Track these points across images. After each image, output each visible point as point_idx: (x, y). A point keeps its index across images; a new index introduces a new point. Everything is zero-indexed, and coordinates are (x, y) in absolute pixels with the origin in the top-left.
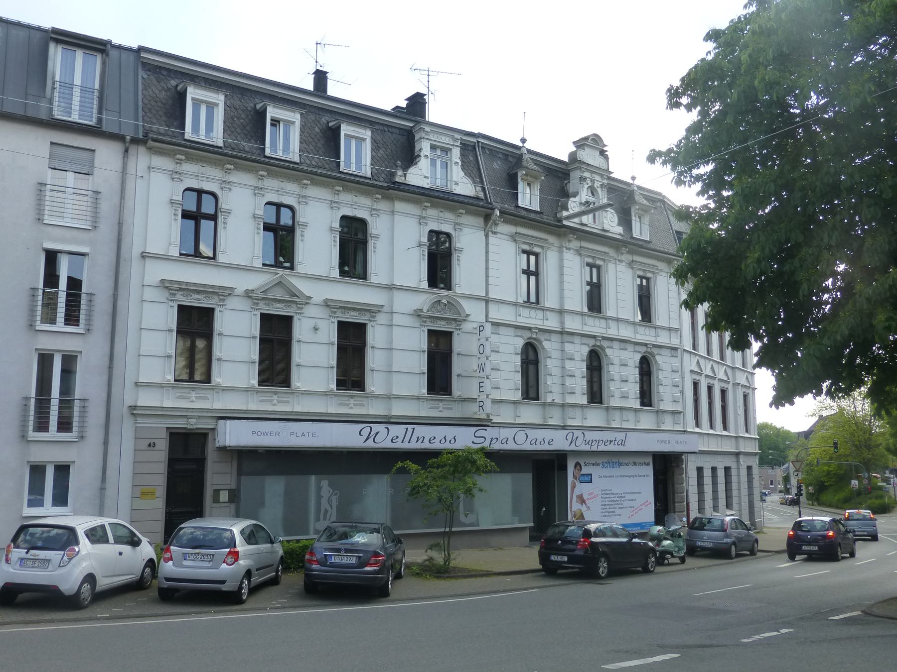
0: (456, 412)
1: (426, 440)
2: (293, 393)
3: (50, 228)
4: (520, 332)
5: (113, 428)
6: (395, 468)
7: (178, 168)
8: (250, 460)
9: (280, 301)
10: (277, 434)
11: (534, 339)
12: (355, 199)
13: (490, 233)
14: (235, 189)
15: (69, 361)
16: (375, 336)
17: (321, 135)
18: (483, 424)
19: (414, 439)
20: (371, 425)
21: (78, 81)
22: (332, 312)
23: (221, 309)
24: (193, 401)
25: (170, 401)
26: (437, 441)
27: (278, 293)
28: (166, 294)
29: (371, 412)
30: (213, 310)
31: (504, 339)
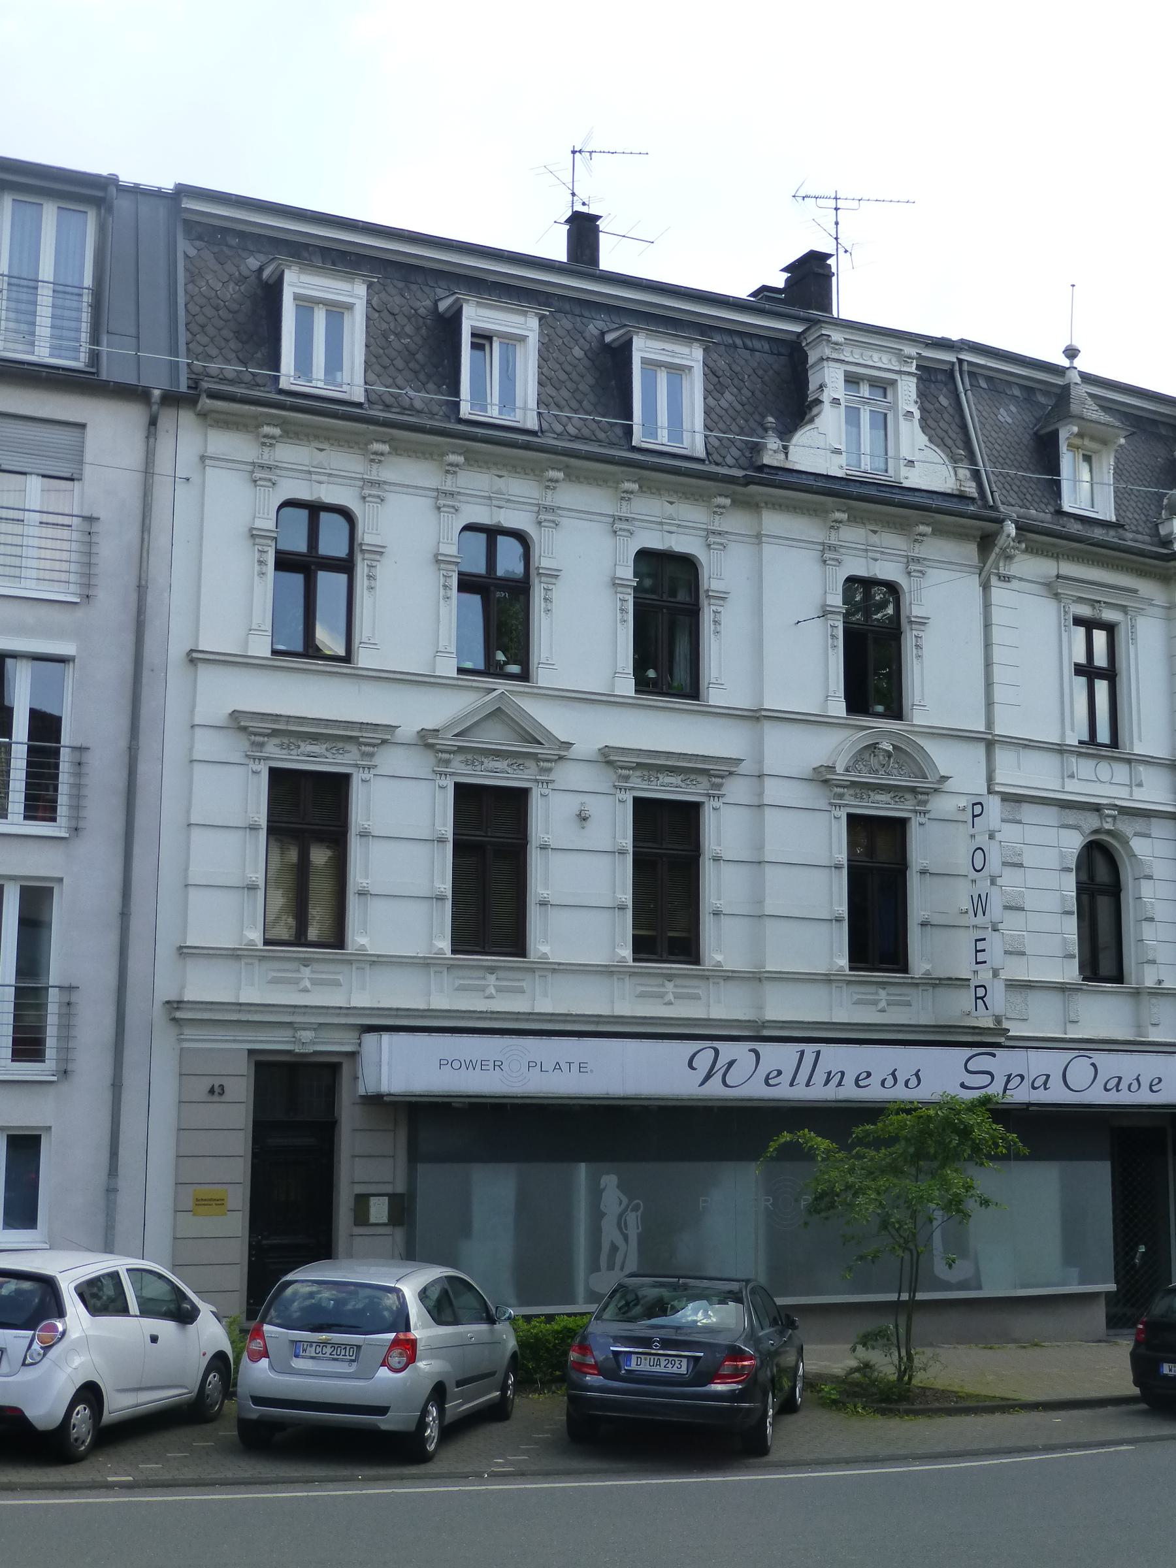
0: (920, 1011)
1: (849, 1080)
4: (1072, 817)
5: (132, 1054)
7: (267, 457)
8: (447, 1128)
9: (497, 754)
11: (1109, 832)
13: (994, 581)
14: (392, 498)
16: (722, 832)
18: (988, 1040)
19: (819, 1077)
20: (716, 1044)
21: (46, 271)
23: (366, 776)
25: (255, 989)
26: (875, 1080)
27: (495, 737)
31: (1033, 834)
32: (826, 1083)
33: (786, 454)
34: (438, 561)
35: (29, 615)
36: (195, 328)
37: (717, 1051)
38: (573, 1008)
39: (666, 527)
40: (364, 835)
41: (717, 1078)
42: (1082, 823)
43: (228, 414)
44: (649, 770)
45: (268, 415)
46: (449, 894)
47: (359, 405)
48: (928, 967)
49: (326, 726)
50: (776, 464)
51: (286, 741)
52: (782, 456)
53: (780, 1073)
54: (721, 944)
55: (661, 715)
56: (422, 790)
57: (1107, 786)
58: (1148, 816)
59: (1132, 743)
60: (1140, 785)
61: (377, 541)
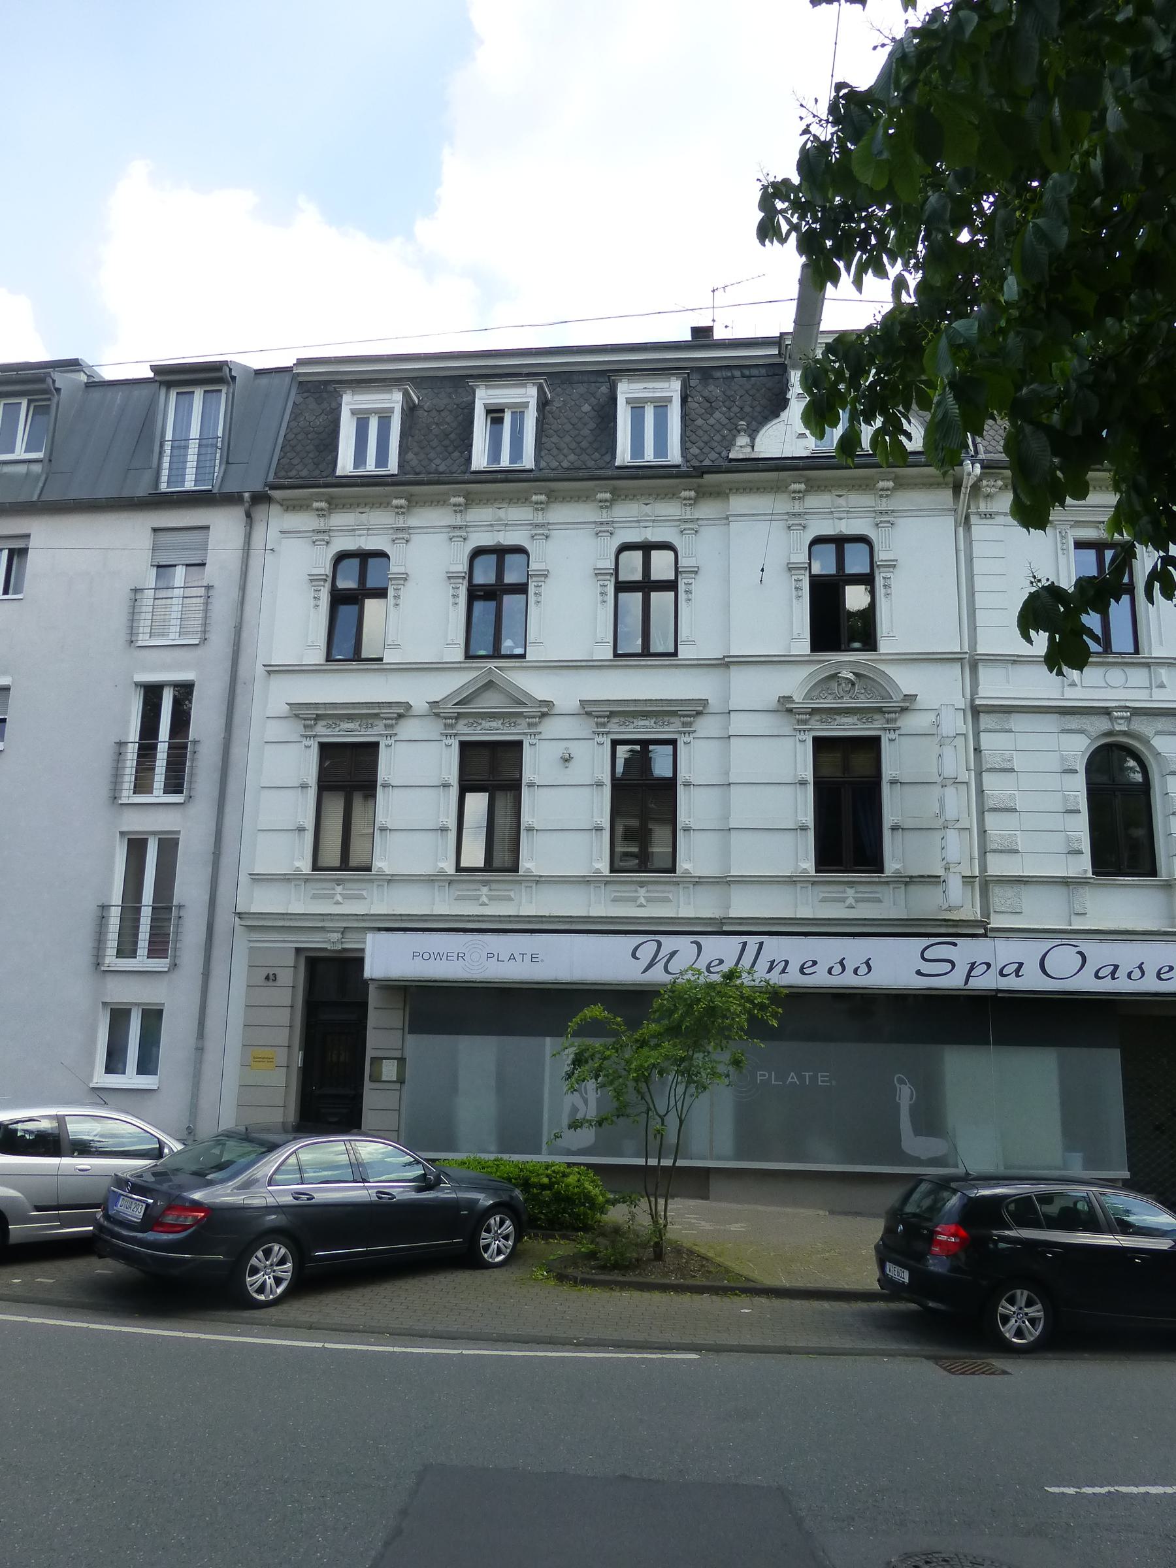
0: (889, 905)
1: (793, 968)
2: (677, 884)
3: (146, 652)
4: (1074, 722)
5: (219, 952)
6: (577, 1019)
7: (884, 505)
8: (440, 1007)
9: (493, 716)
10: (461, 956)
11: (1125, 733)
12: (647, 509)
13: (974, 519)
14: (416, 539)
15: (169, 846)
16: (695, 763)
17: (593, 414)
18: (952, 930)
20: (658, 937)
21: (195, 432)
22: (799, 722)
23: (687, 739)
24: (641, 906)
25: (298, 903)
26: (822, 969)
27: (490, 702)
28: (591, 723)
29: (683, 913)
30: (519, 744)
31: (1023, 741)
33: (753, 447)
34: (790, 569)
35: (167, 655)
36: (288, 448)
37: (659, 944)
38: (566, 908)
39: (836, 515)
40: (386, 786)
41: (660, 966)
42: (1088, 728)
43: (854, 479)
45: (317, 494)
46: (811, 824)
47: (531, 471)
48: (898, 867)
49: (354, 708)
50: (741, 456)
51: (471, 720)
52: (749, 449)
54: (694, 856)
55: (337, 676)
56: (294, 751)
57: (1121, 690)
58: (1010, 712)
59: (1150, 648)
60: (1162, 686)
61: (542, 566)
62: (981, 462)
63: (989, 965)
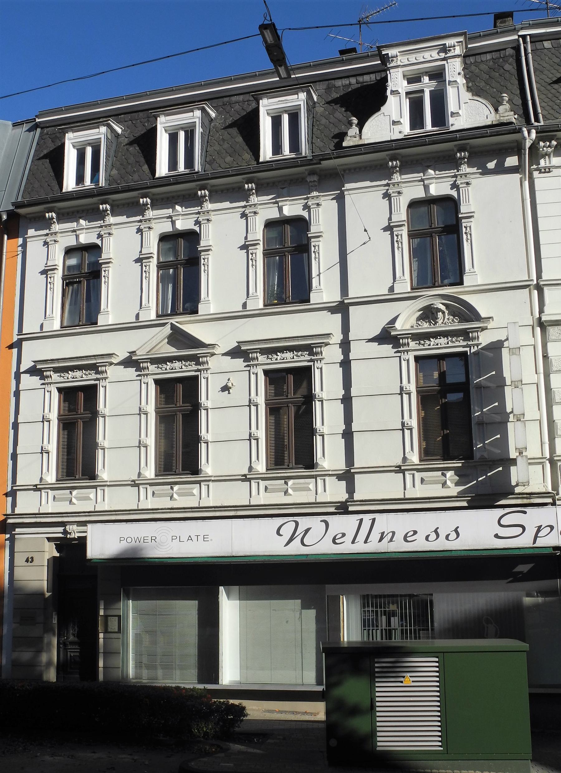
1: (399, 537)
13: (536, 174)
19: (375, 536)
20: (296, 518)
32: (380, 540)
41: (297, 541)
44: (452, 336)
53: (344, 535)
62: (536, 128)
63: (552, 528)
